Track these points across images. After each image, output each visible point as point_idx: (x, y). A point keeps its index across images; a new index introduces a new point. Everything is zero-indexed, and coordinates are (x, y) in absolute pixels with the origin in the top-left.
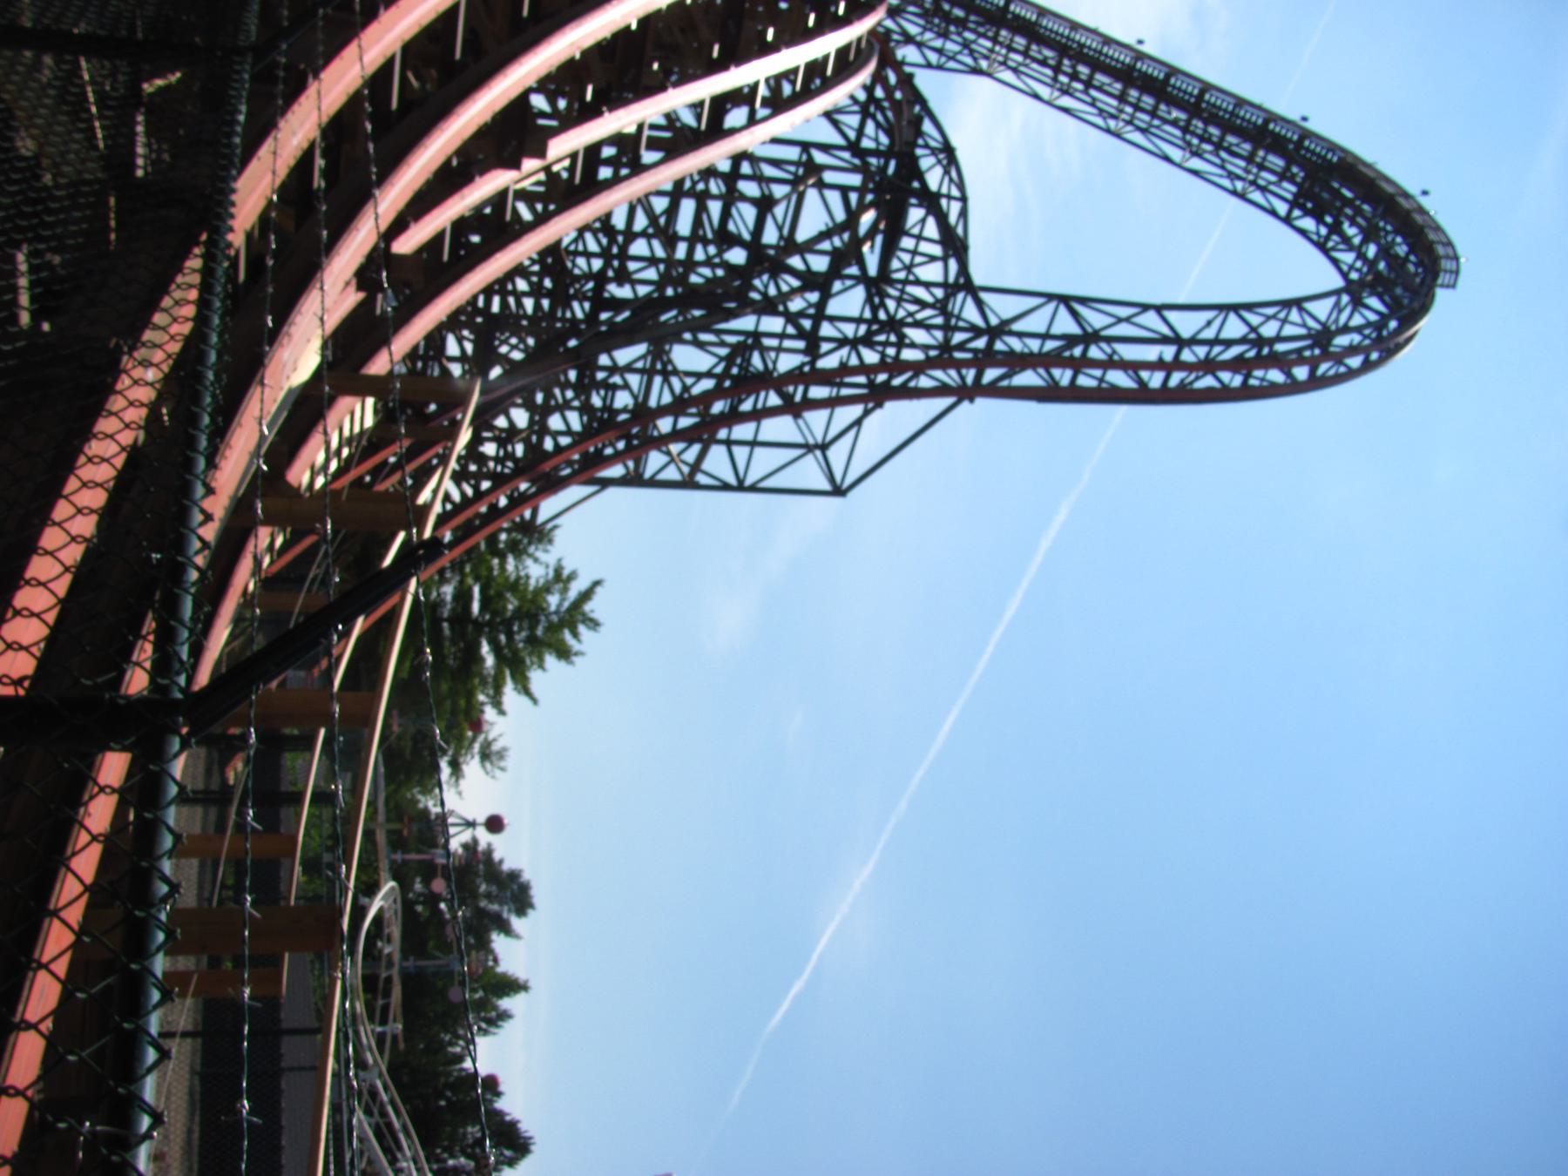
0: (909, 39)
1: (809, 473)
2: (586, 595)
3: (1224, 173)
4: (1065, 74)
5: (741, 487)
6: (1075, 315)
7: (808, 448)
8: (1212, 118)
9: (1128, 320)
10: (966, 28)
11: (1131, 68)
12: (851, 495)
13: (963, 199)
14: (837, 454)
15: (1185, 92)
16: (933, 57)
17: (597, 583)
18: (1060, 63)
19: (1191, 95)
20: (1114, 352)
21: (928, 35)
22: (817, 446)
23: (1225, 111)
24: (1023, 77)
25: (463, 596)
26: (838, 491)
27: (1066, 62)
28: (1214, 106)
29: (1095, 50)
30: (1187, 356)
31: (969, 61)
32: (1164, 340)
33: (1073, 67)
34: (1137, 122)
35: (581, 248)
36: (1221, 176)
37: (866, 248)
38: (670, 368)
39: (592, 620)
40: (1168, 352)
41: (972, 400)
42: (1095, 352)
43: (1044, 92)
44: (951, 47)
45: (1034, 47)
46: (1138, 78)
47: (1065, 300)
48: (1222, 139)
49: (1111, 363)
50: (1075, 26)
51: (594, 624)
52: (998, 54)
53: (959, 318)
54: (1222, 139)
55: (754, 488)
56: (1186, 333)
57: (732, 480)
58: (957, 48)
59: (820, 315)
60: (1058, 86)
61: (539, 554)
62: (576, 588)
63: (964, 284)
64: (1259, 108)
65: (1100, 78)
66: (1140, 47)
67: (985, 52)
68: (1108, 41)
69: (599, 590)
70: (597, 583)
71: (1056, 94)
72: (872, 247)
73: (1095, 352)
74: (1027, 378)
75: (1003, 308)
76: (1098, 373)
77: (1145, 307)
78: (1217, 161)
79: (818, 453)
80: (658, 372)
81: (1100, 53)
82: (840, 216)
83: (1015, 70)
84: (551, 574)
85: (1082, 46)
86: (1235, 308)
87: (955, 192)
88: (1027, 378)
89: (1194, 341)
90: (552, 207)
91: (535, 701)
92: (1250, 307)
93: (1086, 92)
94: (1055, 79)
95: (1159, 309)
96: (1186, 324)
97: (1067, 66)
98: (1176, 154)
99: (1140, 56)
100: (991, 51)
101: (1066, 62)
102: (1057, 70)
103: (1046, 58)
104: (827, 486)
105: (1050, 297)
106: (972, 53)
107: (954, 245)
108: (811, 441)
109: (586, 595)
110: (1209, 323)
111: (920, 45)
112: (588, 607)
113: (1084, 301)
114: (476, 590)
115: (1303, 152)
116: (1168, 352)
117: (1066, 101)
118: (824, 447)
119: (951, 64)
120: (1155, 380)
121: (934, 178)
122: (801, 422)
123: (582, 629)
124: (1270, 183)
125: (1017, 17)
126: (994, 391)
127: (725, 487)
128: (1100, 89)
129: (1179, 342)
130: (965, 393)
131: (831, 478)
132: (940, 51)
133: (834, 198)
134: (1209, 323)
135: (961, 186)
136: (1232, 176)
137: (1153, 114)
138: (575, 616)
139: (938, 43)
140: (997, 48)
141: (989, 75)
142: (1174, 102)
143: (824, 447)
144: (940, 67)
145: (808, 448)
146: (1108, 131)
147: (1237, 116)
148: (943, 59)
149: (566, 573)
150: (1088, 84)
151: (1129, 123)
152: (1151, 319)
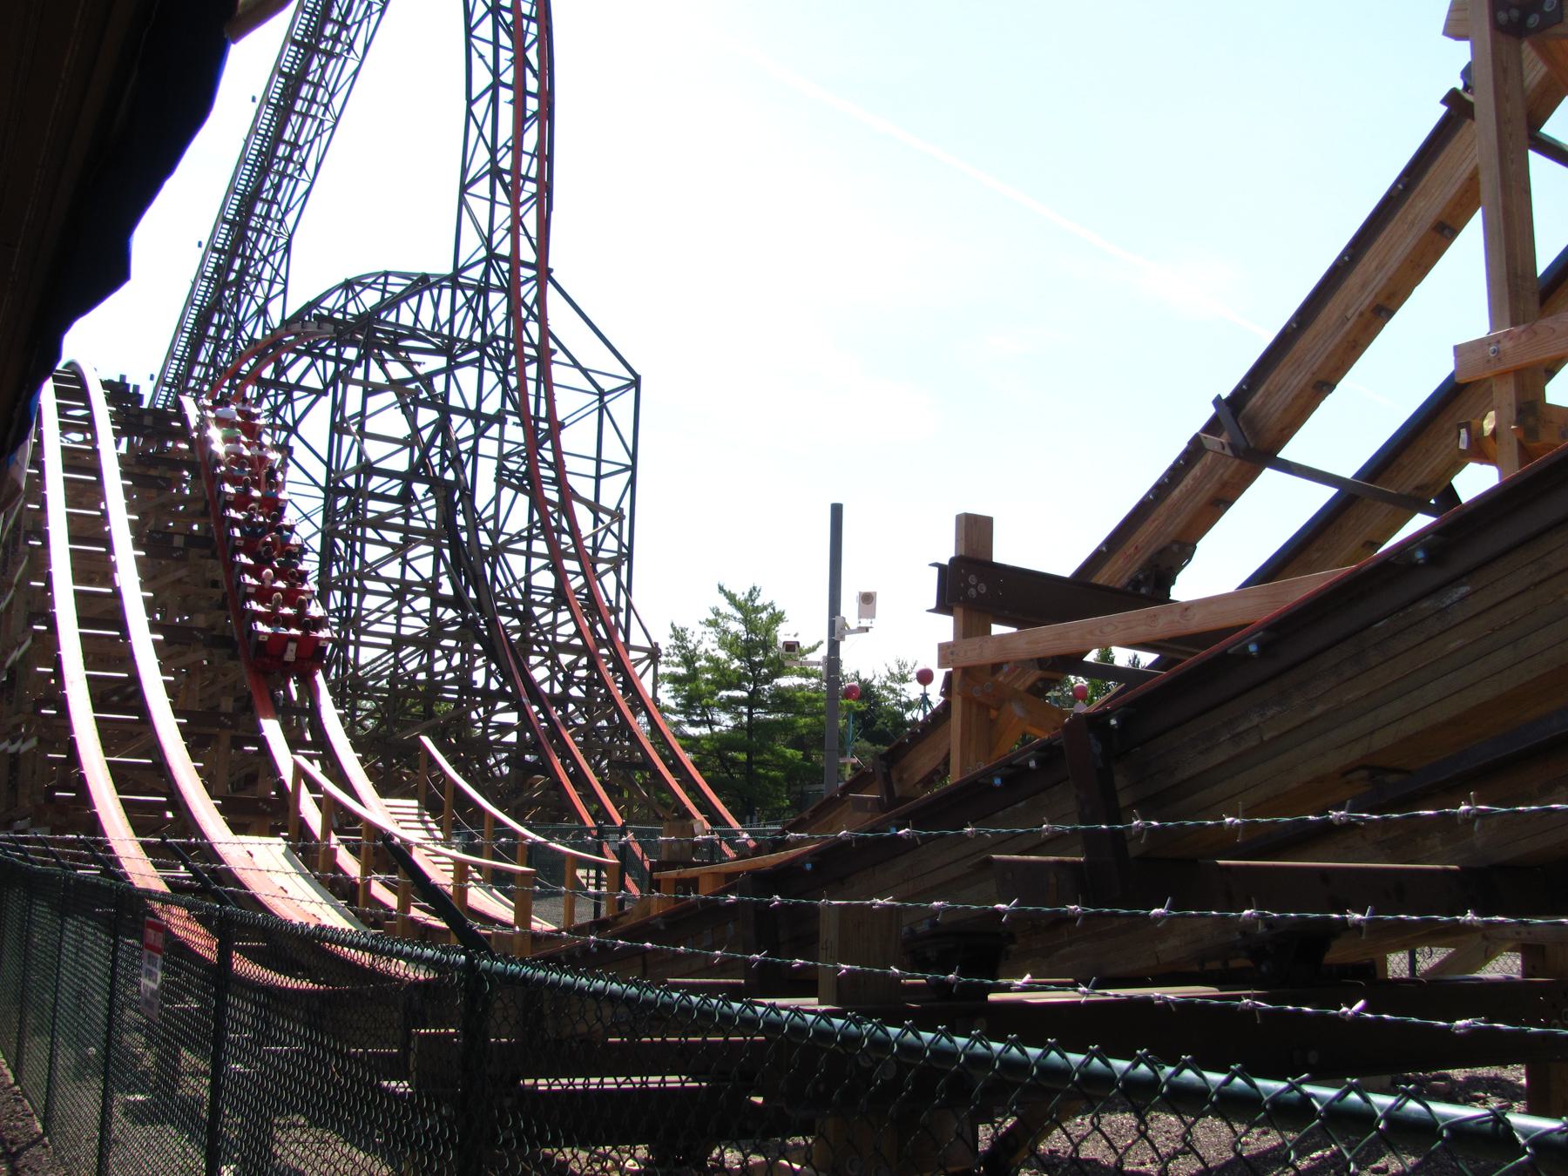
0: (263, 311)
1: (621, 407)
2: (731, 598)
3: (318, 139)
4: (334, 47)
5: (633, 468)
6: (474, 181)
7: (602, 408)
8: (316, 33)
9: (480, 128)
10: (251, 257)
11: (277, 107)
12: (638, 373)
13: (386, 274)
14: (607, 384)
15: (295, 58)
16: (277, 288)
17: (721, 589)
18: (325, 52)
19: (297, 53)
20: (505, 145)
21: (259, 292)
22: (601, 400)
23: (310, 20)
24: (291, 206)
25: (729, 705)
26: (636, 383)
27: (322, 46)
28: (305, 31)
29: (263, 141)
30: (508, 77)
31: (279, 255)
32: (495, 101)
33: (327, 39)
34: (325, 101)
35: (427, 614)
36: (369, 22)
37: (421, 370)
38: (525, 534)
39: (751, 594)
40: (506, 95)
41: (551, 270)
42: (506, 164)
43: (351, 66)
44: (267, 274)
45: (310, 78)
46: (286, 103)
47: (464, 188)
48: (336, 22)
49: (517, 148)
50: (243, 160)
51: (753, 592)
52: (271, 229)
53: (481, 281)
54: (336, 22)
55: (634, 457)
56: (489, 79)
57: (629, 473)
58: (268, 267)
59: (475, 415)
60: (345, 54)
61: (695, 641)
62: (726, 608)
63: (454, 280)
64: (194, 284)
65: (288, 135)
66: (204, 246)
67: (270, 241)
68: (254, 130)
69: (727, 588)
70: (721, 589)
71: (304, 175)
72: (419, 364)
73: (506, 164)
74: (530, 221)
75: (472, 246)
76: (526, 159)
77: (469, 113)
78: (355, 28)
79: (606, 398)
80: (529, 546)
81: (265, 136)
82: (390, 397)
83: (332, 95)
84: (712, 629)
85: (260, 152)
86: (469, 31)
87: (382, 280)
88: (530, 221)
89: (495, 72)
90: (539, 458)
91: (931, 565)
92: (468, 15)
93: (301, 148)
94: (291, 177)
95: (470, 102)
96: (482, 78)
97: (327, 45)
98: (351, 66)
99: (266, 100)
100: (269, 235)
101: (322, 46)
102: (330, 55)
103: (320, 66)
104: (633, 391)
105: (462, 202)
106: (272, 253)
107: (421, 284)
108: (597, 404)
109: (731, 598)
110: (481, 56)
111: (268, 299)
112: (740, 597)
113: (465, 171)
114: (724, 693)
115: (226, 248)
116: (506, 95)
117: (359, 46)
118: (602, 394)
119: (282, 272)
120: (532, 104)
121: (371, 298)
122: (567, 422)
123: (758, 603)
124: (279, 209)
125: (238, 212)
126: (542, 247)
127: (632, 482)
128: (298, 136)
129: (495, 86)
130: (544, 274)
131: (627, 387)
132: (272, 282)
133: (374, 403)
134: (481, 56)
135: (379, 275)
136: (367, 15)
137: (317, 86)
138: (747, 609)
139: (266, 284)
140: (313, 112)
141: (291, 236)
142: (305, 70)
143: (602, 394)
144: (286, 282)
145: (602, 408)
146: (334, 127)
147: (183, 356)
148: (278, 279)
149: (712, 617)
150: (295, 146)
151: (326, 107)
152: (480, 109)
